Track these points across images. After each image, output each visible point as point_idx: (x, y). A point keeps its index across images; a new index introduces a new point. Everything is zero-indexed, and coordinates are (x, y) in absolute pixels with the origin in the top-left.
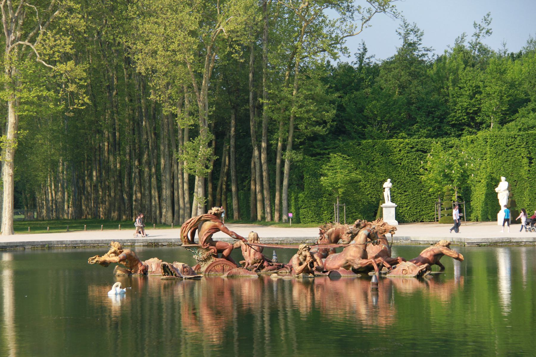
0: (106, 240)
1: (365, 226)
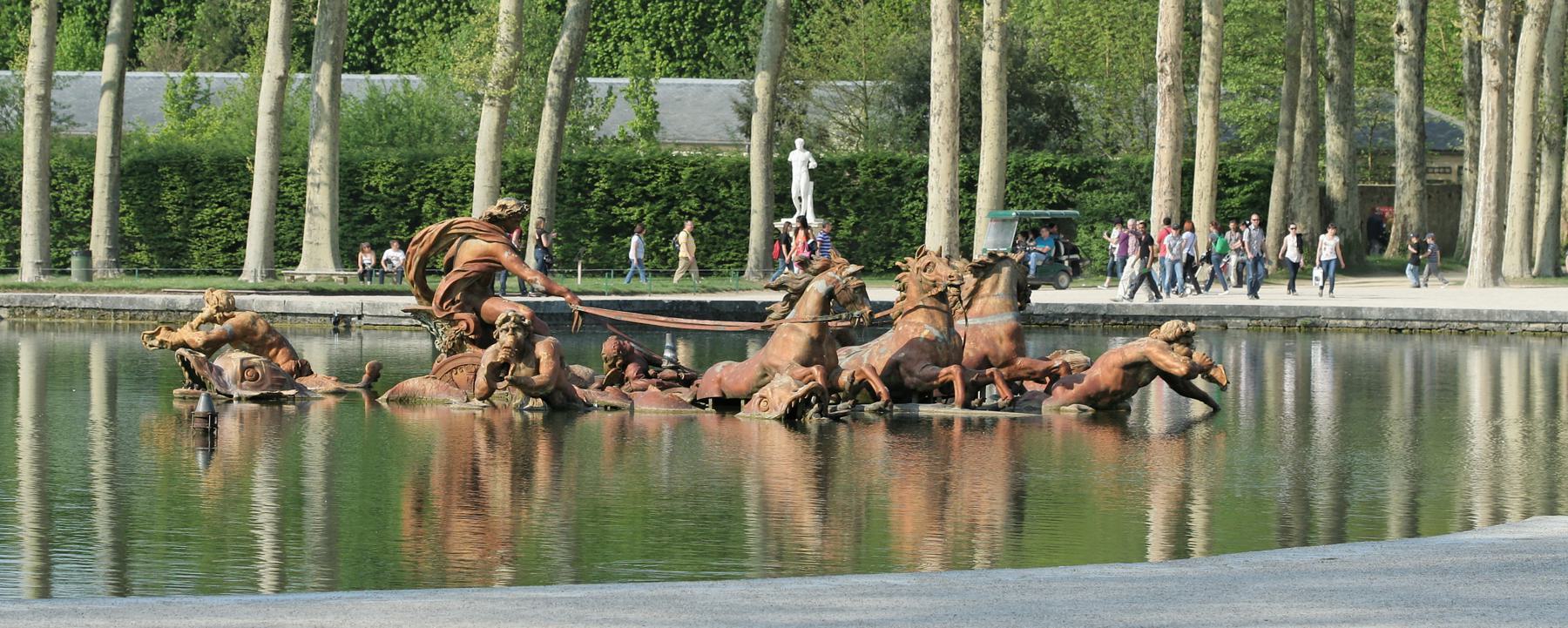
0: (1504, 312)
1: (825, 268)
